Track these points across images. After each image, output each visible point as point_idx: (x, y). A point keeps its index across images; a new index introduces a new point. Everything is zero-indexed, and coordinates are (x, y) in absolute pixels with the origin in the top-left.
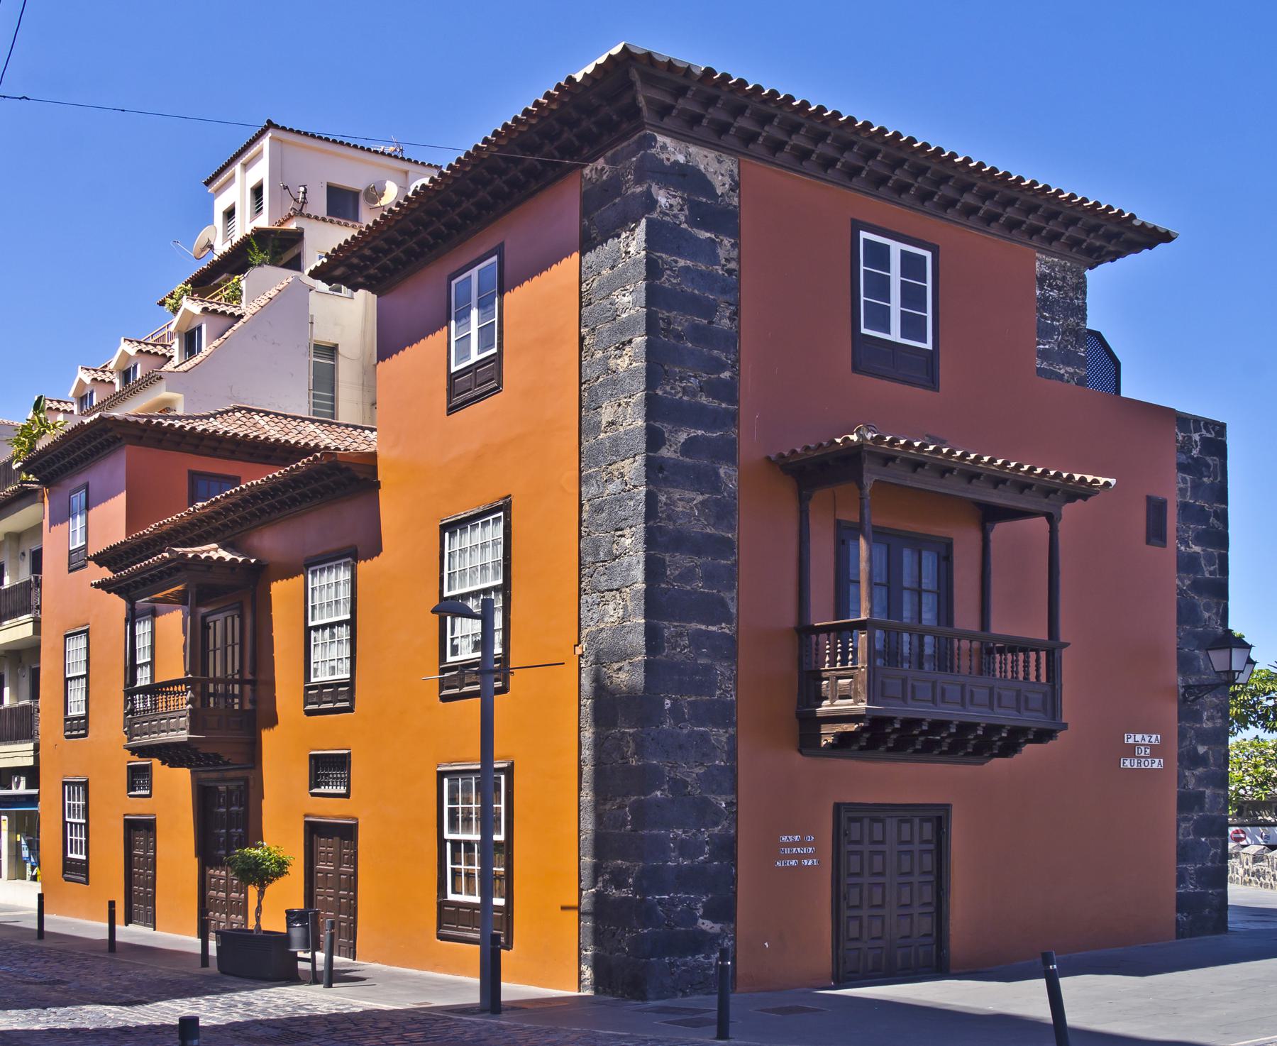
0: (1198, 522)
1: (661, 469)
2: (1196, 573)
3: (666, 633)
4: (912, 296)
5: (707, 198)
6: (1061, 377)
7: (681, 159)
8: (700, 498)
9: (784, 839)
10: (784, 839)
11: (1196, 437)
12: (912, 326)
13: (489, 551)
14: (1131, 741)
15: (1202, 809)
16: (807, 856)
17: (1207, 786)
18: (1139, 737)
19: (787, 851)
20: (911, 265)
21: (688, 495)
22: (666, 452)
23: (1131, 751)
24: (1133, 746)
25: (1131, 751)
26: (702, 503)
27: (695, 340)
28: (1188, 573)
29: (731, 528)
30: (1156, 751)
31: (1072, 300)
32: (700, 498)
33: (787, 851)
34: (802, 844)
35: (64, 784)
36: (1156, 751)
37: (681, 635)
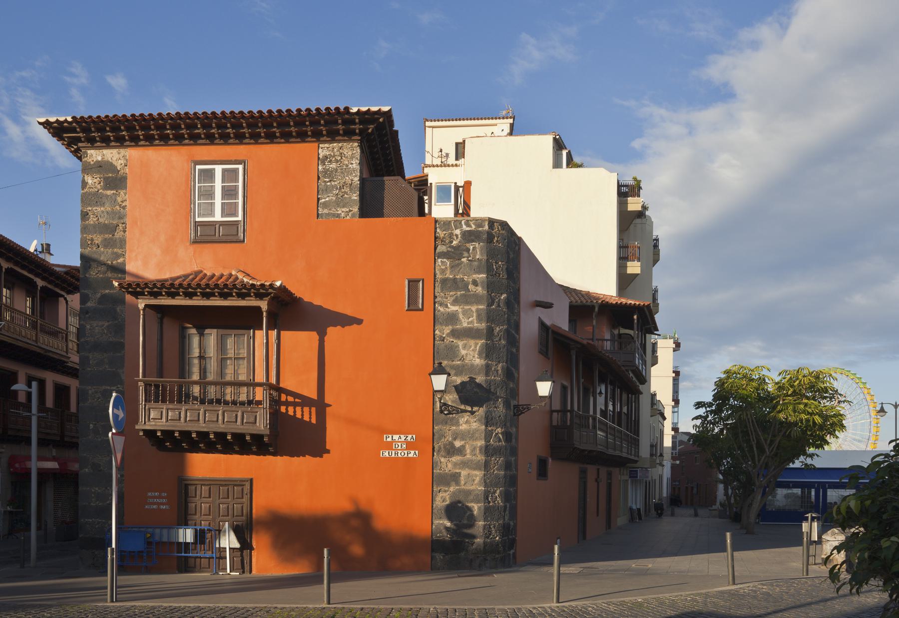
0: (457, 288)
1: (87, 313)
2: (456, 324)
3: (90, 392)
4: (229, 193)
5: (112, 173)
6: (338, 216)
7: (100, 158)
8: (106, 324)
9: (149, 494)
10: (149, 494)
11: (458, 232)
12: (229, 209)
13: (345, 151)
14: (389, 439)
15: (457, 483)
16: (163, 504)
17: (462, 468)
18: (396, 437)
19: (151, 500)
20: (230, 175)
21: (100, 323)
22: (89, 304)
23: (389, 446)
24: (391, 443)
25: (389, 446)
26: (108, 326)
27: (105, 246)
28: (446, 326)
29: (450, 186)
30: (410, 446)
31: (347, 166)
32: (106, 324)
33: (151, 500)
34: (160, 497)
35: (422, 310)
36: (410, 446)
37: (96, 392)
